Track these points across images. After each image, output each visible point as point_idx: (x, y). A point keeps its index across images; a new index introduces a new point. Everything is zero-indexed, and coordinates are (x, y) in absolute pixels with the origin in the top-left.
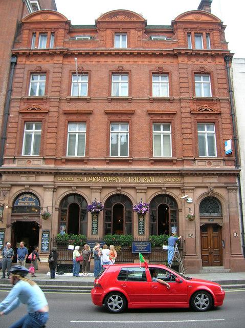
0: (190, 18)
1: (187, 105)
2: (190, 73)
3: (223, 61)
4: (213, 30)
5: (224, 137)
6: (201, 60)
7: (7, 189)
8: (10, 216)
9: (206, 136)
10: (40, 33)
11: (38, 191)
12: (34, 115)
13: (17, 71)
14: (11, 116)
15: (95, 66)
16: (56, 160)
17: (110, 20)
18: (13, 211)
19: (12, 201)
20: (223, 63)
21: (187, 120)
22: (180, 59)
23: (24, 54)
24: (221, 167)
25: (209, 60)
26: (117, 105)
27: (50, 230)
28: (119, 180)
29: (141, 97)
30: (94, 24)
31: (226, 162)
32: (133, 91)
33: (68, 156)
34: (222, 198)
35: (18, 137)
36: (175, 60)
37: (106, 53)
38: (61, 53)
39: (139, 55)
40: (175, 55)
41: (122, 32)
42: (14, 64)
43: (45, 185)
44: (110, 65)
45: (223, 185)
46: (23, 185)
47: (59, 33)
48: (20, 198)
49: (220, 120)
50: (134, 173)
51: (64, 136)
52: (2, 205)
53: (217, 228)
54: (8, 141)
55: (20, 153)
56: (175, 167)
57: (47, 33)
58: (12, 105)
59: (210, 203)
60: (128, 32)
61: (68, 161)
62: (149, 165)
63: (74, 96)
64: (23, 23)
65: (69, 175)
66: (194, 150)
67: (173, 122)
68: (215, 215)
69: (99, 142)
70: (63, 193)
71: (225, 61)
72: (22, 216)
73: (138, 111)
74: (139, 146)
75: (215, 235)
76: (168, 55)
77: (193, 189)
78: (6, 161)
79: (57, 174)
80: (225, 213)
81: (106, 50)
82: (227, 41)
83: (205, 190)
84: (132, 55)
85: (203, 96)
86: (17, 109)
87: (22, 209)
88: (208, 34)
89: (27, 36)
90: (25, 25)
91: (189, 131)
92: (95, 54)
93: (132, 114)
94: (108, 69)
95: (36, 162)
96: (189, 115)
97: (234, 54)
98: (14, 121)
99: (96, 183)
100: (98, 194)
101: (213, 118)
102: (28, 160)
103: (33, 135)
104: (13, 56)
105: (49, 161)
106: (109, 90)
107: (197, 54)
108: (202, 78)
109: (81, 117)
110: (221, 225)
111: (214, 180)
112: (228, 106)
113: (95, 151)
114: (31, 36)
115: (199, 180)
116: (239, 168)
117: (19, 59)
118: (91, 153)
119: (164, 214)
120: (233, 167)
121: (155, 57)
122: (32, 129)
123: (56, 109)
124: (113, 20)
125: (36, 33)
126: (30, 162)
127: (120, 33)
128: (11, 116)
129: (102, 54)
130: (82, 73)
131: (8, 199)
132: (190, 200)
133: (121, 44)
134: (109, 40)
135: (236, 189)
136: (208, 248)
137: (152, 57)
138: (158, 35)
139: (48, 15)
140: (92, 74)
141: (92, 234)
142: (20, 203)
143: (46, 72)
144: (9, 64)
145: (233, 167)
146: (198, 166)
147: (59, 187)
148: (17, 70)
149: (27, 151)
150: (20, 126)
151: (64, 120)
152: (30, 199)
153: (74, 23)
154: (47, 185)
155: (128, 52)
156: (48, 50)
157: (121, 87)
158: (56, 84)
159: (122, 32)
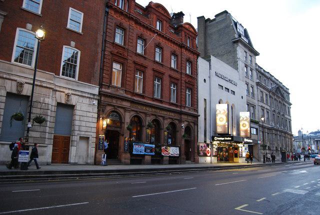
152: (116, 116)
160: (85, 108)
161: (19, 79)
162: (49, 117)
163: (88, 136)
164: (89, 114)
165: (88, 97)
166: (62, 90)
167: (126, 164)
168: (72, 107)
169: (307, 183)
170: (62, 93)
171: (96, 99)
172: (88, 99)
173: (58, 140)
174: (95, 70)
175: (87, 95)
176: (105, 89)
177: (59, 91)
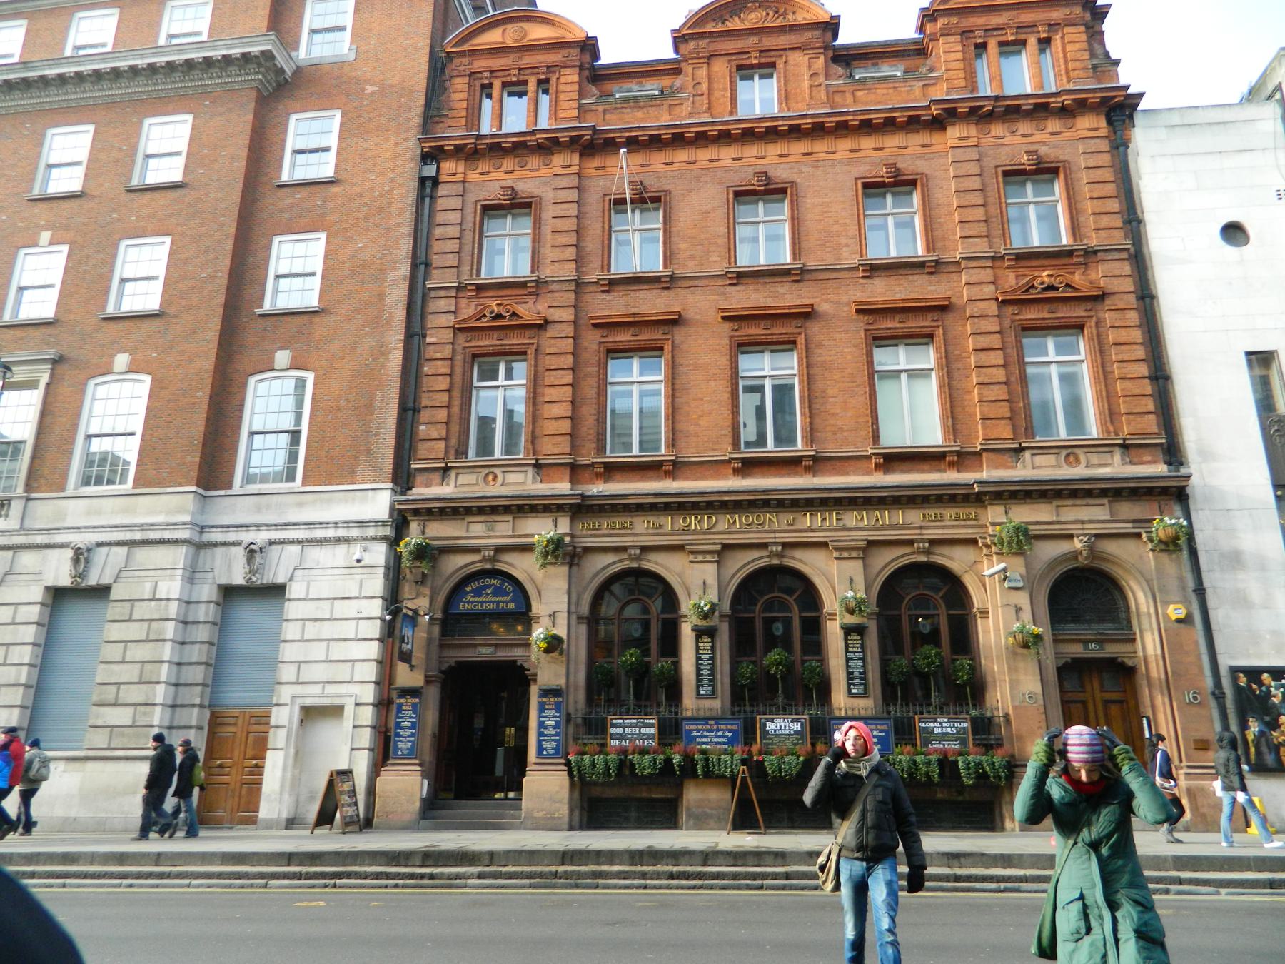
3: (1103, 122)
6: (1024, 127)
8: (435, 648)
9: (1054, 371)
10: (504, 85)
13: (441, 203)
14: (428, 340)
15: (681, 176)
17: (720, 28)
18: (445, 632)
20: (1104, 131)
23: (459, 149)
25: (1053, 125)
29: (829, 261)
31: (1133, 452)
33: (612, 456)
35: (457, 403)
36: (936, 138)
37: (713, 131)
38: (574, 141)
39: (819, 130)
40: (938, 120)
41: (760, 66)
42: (429, 184)
44: (726, 169)
45: (1128, 527)
47: (563, 79)
48: (469, 589)
50: (821, 499)
51: (598, 394)
52: (410, 613)
54: (425, 416)
55: (462, 452)
56: (952, 476)
57: (525, 83)
58: (433, 306)
59: (1082, 594)
61: (611, 470)
65: (537, 512)
69: (706, 407)
71: (1110, 122)
75: (1114, 696)
79: (581, 509)
81: (713, 123)
82: (1114, 56)
84: (795, 132)
85: (1036, 243)
86: (448, 320)
87: (479, 621)
88: (1045, 43)
89: (464, 96)
90: (456, 61)
92: (678, 140)
94: (720, 183)
95: (513, 477)
96: (993, 308)
97: (1141, 95)
98: (438, 356)
99: (704, 533)
101: (1078, 312)
104: (426, 157)
105: (552, 471)
106: (733, 429)
107: (1009, 110)
108: (1029, 187)
109: (650, 336)
110: (1129, 663)
111: (1095, 514)
112: (1127, 269)
113: (696, 435)
114: (478, 94)
116: (1183, 471)
117: (447, 166)
118: (681, 443)
119: (922, 624)
120: (1161, 469)
122: (496, 379)
125: (490, 85)
126: (495, 477)
127: (752, 66)
128: (428, 340)
129: (701, 139)
130: (646, 199)
133: (759, 99)
134: (722, 97)
138: (875, 65)
139: (525, 25)
140: (674, 203)
141: (699, 696)
142: (469, 604)
144: (413, 184)
145: (1161, 469)
146: (1027, 469)
148: (440, 201)
150: (458, 370)
152: (498, 591)
155: (783, 125)
156: (533, 133)
157: (765, 241)
158: (563, 239)
159: (760, 66)
160: (324, 585)
161: (246, 537)
162: (170, 635)
163: (337, 701)
164: (342, 609)
165: (338, 540)
166: (231, 537)
167: (549, 825)
168: (277, 591)
169: (1147, 735)
170: (233, 549)
171: (375, 539)
172: (341, 549)
173: (232, 729)
174: (374, 425)
175: (330, 533)
176: (428, 485)
177: (225, 544)
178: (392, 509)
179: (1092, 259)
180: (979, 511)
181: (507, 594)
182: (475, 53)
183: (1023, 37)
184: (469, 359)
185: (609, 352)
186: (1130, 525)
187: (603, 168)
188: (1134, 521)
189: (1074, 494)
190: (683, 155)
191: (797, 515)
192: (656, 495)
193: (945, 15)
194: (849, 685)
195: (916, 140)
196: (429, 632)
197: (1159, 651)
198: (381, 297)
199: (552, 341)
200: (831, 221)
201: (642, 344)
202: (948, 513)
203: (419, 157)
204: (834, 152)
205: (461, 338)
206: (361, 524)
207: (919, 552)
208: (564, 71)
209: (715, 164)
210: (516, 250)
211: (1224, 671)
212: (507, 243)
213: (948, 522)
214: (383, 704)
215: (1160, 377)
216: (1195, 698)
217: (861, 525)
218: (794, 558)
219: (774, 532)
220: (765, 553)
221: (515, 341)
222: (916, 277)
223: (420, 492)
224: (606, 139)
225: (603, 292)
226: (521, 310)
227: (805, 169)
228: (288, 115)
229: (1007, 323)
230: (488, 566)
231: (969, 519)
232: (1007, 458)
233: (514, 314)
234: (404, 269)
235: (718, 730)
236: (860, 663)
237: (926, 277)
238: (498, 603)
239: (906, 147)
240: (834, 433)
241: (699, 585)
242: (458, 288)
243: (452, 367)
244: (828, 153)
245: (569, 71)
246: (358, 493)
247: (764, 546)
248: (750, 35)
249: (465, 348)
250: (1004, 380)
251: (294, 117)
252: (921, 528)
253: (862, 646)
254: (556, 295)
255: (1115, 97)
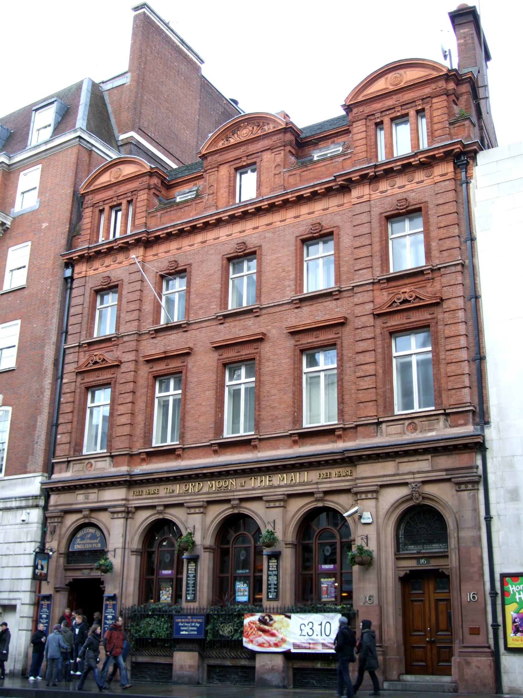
0: (380, 85)
1: (367, 297)
2: (375, 219)
4: (430, 97)
5: (448, 358)
6: (400, 181)
7: (56, 520)
11: (102, 518)
12: (99, 373)
13: (75, 292)
16: (131, 456)
19: (64, 541)
21: (366, 334)
22: (355, 193)
23: (364, 177)
24: (442, 431)
25: (419, 176)
26: (235, 326)
27: (118, 595)
28: (233, 483)
30: (344, 113)
31: (115, 459)
32: (264, 290)
34: (445, 505)
38: (448, 154)
41: (248, 165)
42: (69, 281)
43: (110, 507)
44: (223, 244)
45: (443, 475)
46: (79, 511)
49: (440, 316)
53: (441, 578)
55: (389, 406)
56: (340, 445)
57: (407, 115)
59: (420, 522)
60: (258, 160)
62: (291, 447)
63: (310, 291)
64: (83, 196)
66: (381, 401)
67: (338, 343)
68: (436, 548)
69: (203, 409)
70: (144, 518)
72: (81, 569)
73: (273, 333)
74: (274, 408)
76: (329, 192)
77: (376, 492)
78: (57, 468)
79: (131, 483)
80: (453, 542)
83: (404, 491)
90: (87, 198)
91: (369, 357)
93: (260, 339)
96: (370, 320)
99: (196, 494)
100: (198, 517)
101: (423, 316)
102: (87, 461)
103: (243, 388)
105: (120, 459)
111: (422, 466)
113: (196, 429)
115: (387, 468)
118: (188, 436)
121: (306, 203)
123: (131, 356)
124: (232, 141)
125: (382, 122)
131: (57, 538)
132: (367, 517)
135: (478, 483)
136: (425, 630)
137: (301, 205)
142: (78, 546)
143: (419, 210)
144: (61, 282)
145: (469, 429)
146: (390, 436)
147: (138, 508)
149: (408, 404)
151: (146, 375)
152: (93, 537)
153: (302, 121)
154: (114, 506)
159: (248, 165)
175: (14, 504)
176: (60, 472)
178: (42, 489)
179: (436, 274)
180: (353, 469)
181: (97, 538)
182: (93, 192)
183: (406, 111)
184: (151, 380)
185: (391, 334)
186: (444, 473)
187: (157, 255)
188: (446, 470)
189: (407, 454)
190: (199, 238)
191: (247, 479)
192: (168, 472)
193: (356, 107)
194: (268, 592)
195: (333, 203)
196: (57, 562)
197: (458, 564)
198: (42, 356)
199: (123, 375)
200: (281, 270)
201: (243, 358)
202: (334, 472)
203: (63, 265)
204: (284, 220)
205: (379, 322)
206: (26, 498)
207: (317, 500)
208: (435, 100)
209: (217, 241)
210: (414, 244)
211: (497, 577)
212: (408, 240)
213: (335, 478)
214: (37, 605)
215: (479, 358)
216: (474, 597)
217: (282, 483)
218: (327, 501)
219: (233, 491)
220: (154, 512)
221: (105, 376)
222: (329, 303)
223: (56, 476)
224: (155, 237)
225: (153, 338)
226: (421, 293)
227: (268, 235)
228: (8, 249)
229: (378, 331)
230: (87, 521)
231: (347, 475)
232: (372, 428)
233: (104, 360)
234: (53, 338)
235: (192, 622)
236: (275, 578)
237: (335, 302)
238: (92, 544)
239: (328, 209)
240: (273, 420)
241: (199, 527)
242: (79, 346)
243: (74, 397)
244: (281, 221)
245: (142, 192)
246: (27, 479)
247: (228, 501)
248: (241, 146)
249: (81, 384)
250: (373, 373)
251: (10, 250)
252: (317, 483)
253: (277, 567)
254: (127, 344)
255: (453, 150)
